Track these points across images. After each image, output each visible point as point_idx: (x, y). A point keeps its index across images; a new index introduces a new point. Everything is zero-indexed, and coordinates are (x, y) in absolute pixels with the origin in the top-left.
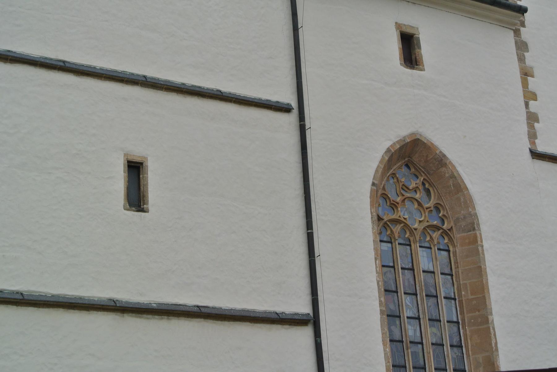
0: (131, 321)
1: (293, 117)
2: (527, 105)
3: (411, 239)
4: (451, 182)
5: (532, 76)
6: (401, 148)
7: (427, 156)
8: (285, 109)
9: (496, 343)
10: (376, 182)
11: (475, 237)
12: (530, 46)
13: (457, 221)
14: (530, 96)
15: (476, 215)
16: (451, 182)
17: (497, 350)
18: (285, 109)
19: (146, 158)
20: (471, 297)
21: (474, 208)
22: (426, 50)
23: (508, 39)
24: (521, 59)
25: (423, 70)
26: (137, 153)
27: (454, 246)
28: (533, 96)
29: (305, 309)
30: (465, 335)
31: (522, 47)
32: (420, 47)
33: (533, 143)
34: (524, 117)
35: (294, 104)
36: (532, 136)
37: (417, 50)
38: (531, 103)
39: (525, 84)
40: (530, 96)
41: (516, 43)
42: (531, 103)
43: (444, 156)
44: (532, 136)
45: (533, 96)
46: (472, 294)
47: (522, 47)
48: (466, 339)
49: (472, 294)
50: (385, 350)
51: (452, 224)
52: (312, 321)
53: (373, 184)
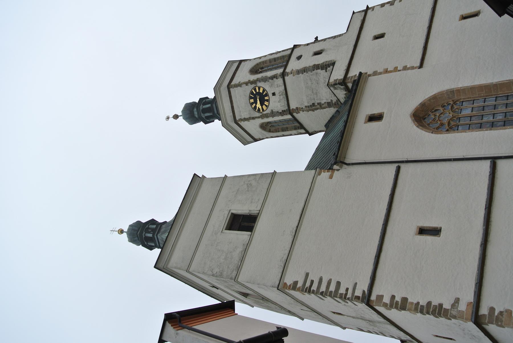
2: (399, 71)
6: (417, 121)
11: (457, 90)
13: (449, 98)
14: (396, 70)
17: (509, 80)
22: (376, 111)
24: (380, 73)
26: (414, 230)
27: (461, 99)
31: (375, 73)
33: (416, 68)
35: (397, 165)
36: (413, 68)
38: (399, 69)
39: (391, 72)
40: (396, 70)
41: (373, 76)
42: (399, 69)
44: (413, 68)
47: (375, 73)
52: (494, 160)
53: (432, 133)
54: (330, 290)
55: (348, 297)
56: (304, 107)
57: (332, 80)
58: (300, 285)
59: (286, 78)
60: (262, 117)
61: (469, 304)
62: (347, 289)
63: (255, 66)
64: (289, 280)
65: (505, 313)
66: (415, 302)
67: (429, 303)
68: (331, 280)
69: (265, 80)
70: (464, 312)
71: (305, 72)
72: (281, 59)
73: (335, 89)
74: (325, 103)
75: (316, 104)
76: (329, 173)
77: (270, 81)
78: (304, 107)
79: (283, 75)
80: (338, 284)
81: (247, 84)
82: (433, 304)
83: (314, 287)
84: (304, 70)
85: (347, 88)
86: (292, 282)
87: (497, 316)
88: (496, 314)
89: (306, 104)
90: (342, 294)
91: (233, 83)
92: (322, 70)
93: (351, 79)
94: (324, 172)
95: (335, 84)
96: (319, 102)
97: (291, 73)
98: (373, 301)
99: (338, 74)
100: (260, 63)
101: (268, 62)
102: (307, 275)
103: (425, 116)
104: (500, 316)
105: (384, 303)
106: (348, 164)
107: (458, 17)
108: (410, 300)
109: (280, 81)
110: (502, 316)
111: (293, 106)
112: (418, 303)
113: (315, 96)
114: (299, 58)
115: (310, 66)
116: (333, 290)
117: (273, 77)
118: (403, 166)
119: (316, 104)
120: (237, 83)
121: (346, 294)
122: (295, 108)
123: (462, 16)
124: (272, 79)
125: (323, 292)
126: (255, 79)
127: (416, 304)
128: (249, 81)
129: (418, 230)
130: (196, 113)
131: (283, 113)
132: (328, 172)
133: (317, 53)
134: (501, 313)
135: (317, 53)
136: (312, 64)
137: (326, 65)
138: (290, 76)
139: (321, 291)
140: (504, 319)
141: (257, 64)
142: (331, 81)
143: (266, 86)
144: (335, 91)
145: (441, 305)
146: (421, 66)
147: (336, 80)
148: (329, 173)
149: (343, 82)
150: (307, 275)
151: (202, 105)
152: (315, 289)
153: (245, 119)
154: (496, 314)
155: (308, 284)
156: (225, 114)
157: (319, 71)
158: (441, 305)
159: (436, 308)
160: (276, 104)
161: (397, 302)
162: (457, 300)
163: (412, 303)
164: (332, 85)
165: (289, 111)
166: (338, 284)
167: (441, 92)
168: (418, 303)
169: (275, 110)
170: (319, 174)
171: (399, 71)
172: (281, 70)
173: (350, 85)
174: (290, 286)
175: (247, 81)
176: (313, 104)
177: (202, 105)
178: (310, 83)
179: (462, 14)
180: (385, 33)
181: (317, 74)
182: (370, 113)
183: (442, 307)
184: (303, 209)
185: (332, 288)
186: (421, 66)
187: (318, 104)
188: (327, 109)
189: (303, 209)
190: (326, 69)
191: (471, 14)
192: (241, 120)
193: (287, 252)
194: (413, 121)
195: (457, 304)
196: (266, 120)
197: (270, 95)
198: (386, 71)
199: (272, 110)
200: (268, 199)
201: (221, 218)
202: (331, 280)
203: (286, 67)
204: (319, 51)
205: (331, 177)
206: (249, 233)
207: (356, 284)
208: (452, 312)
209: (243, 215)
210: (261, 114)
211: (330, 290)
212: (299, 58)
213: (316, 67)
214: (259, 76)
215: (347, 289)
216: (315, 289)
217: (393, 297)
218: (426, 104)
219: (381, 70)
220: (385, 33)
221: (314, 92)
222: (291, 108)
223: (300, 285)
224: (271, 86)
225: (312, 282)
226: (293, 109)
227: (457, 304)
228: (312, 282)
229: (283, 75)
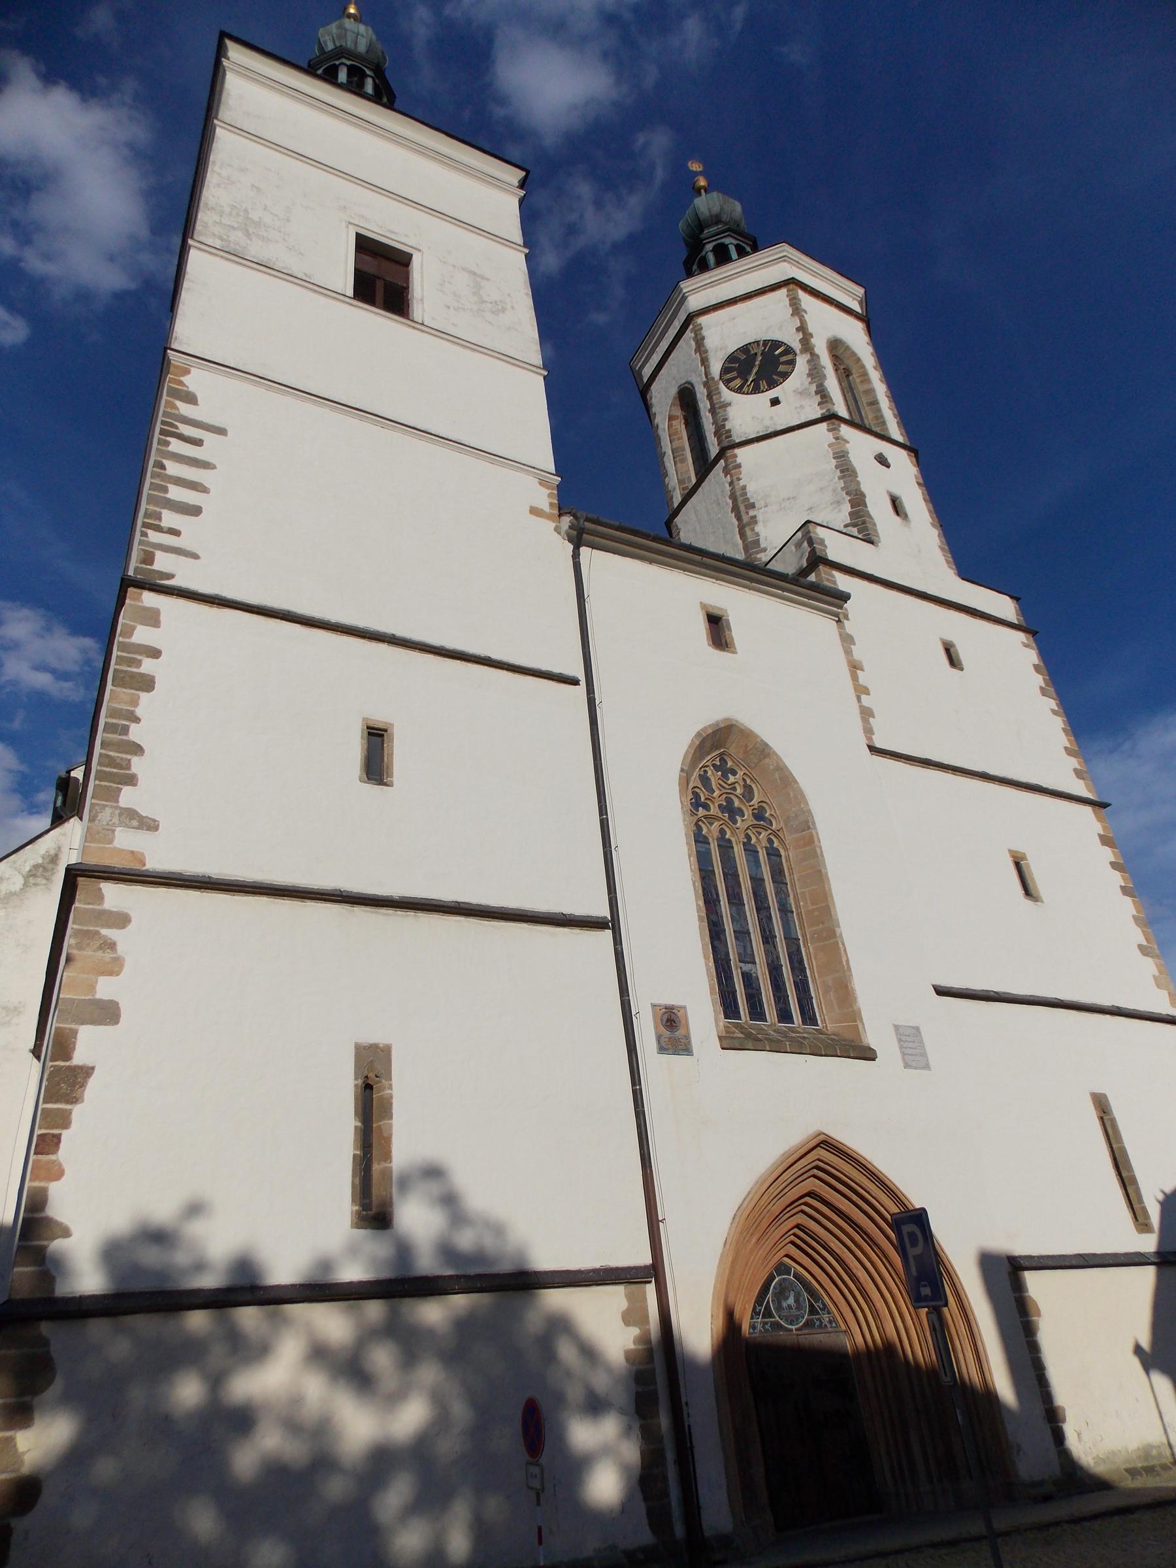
0: (360, 911)
1: (582, 688)
2: (859, 699)
3: (733, 839)
4: (777, 775)
5: (863, 670)
6: (714, 733)
7: (746, 746)
8: (574, 682)
9: (848, 961)
10: (686, 768)
11: (811, 836)
12: (856, 640)
13: (787, 821)
14: (861, 691)
15: (809, 811)
16: (777, 775)
17: (849, 968)
18: (574, 682)
19: (392, 725)
20: (811, 907)
21: (807, 804)
22: (737, 632)
23: (829, 624)
24: (848, 652)
25: (735, 652)
26: (379, 717)
27: (786, 849)
28: (798, 329)
29: (604, 912)
30: (808, 954)
31: (847, 640)
32: (730, 630)
33: (870, 739)
34: (856, 710)
35: (581, 676)
36: (868, 731)
37: (727, 632)
38: (863, 697)
39: (855, 678)
40: (861, 691)
41: (841, 635)
42: (863, 697)
43: (767, 745)
44: (868, 731)
45: (866, 691)
46: (813, 904)
47: (847, 640)
48: (809, 959)
49: (813, 904)
50: (707, 965)
51: (782, 824)
52: (611, 924)
53: (682, 770)
54: (171, 487)
55: (150, 532)
56: (742, 483)
57: (821, 532)
59: (823, 426)
60: (708, 383)
61: (139, 857)
63: (854, 354)
65: (108, 956)
66: (139, 712)
67: (137, 749)
68: (205, 490)
69: (815, 373)
70: (111, 841)
71: (842, 471)
72: (877, 418)
73: (798, 545)
74: (758, 534)
75: (752, 513)
76: (547, 508)
77: (814, 388)
78: (742, 483)
79: (830, 417)
81: (802, 328)
82: (135, 760)
84: (846, 470)
85: (804, 572)
86: (191, 389)
87: (97, 933)
88: (104, 932)
89: (749, 489)
90: (160, 519)
91: (801, 294)
92: (851, 514)
93: (828, 580)
94: (550, 495)
95: (811, 542)
96: (760, 518)
97: (837, 438)
98: (139, 598)
99: (838, 548)
100: (863, 367)
101: (866, 387)
102: (221, 431)
103: (730, 780)
104: (98, 943)
105: (133, 628)
106: (576, 556)
107: (1020, 847)
108: (144, 697)
109: (817, 413)
110: (100, 948)
111: (742, 454)
112: (137, 720)
114: (882, 460)
115: (858, 483)
116: (169, 496)
117: (823, 395)
119: (752, 513)
120: (804, 306)
121: (159, 529)
122: (739, 460)
123: (1024, 858)
125: (163, 467)
126: (817, 350)
127: (132, 713)
128: (811, 335)
129: (381, 726)
130: (713, 229)
131: (721, 431)
132: (551, 504)
134: (112, 946)
135: (896, 505)
136: (864, 488)
137: (864, 522)
138: (830, 438)
139: (166, 462)
140: (88, 952)
141: (859, 360)
142: (819, 530)
143: (799, 377)
144: (792, 547)
145: (131, 780)
146: (873, 749)
147: (822, 542)
148: (547, 508)
149: (817, 560)
150: (221, 431)
151: (736, 242)
152: (170, 448)
153: (700, 342)
154: (104, 932)
155: (185, 430)
156: (712, 284)
157: (847, 508)
158: (131, 780)
159: (122, 768)
160: (746, 412)
161: (139, 663)
162: (150, 825)
163: (135, 702)
164: (809, 532)
165: (728, 447)
166: (195, 511)
167: (803, 796)
168: (137, 720)
169: (732, 412)
170: (543, 483)
172: (843, 412)
173: (812, 578)
175: (810, 330)
176: (753, 506)
177: (736, 242)
179: (1028, 857)
180: (962, 669)
182: (731, 619)
183: (126, 784)
186: (873, 749)
187: (755, 517)
188: (740, 542)
190: (854, 525)
191: (1029, 882)
192: (698, 331)
194: (717, 723)
195: (135, 823)
196: (701, 393)
197: (772, 393)
198: (855, 667)
199: (730, 404)
200: (458, 348)
201: (393, 226)
202: (205, 490)
203: (850, 423)
204: (903, 507)
205: (535, 511)
206: (350, 292)
207: (196, 557)
208: (108, 811)
209: (407, 288)
210: (717, 377)
211: (171, 487)
212: (882, 460)
213: (858, 501)
214: (826, 360)
216: (170, 448)
217: (155, 653)
218: (767, 761)
219: (858, 652)
220: (962, 669)
222: (737, 451)
224: (802, 393)
225: (198, 443)
226: (736, 456)
227: (135, 823)
228: (198, 443)
229: (830, 417)
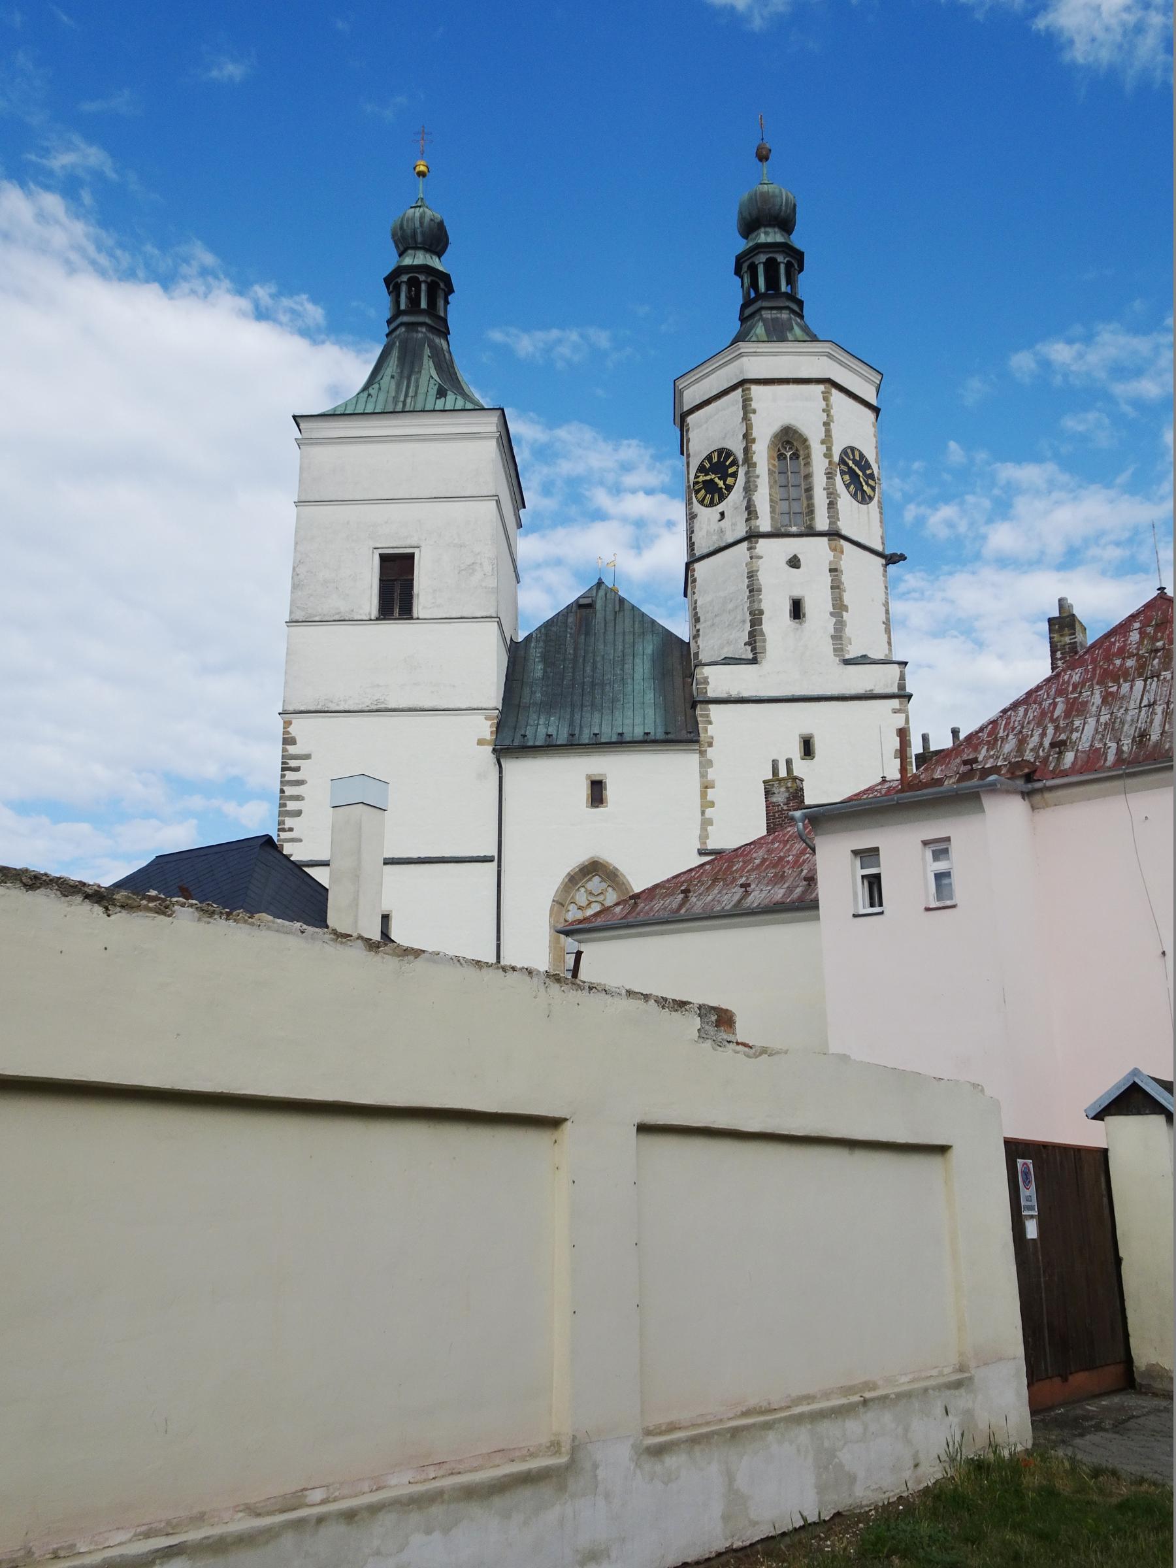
2: (703, 813)
58: (292, 750)
62: (291, 830)
63: (801, 435)
64: (299, 727)
77: (745, 504)
80: (298, 813)
83: (290, 776)
102: (307, 757)
113: (709, 623)
115: (760, 601)
118: (895, 690)
124: (747, 508)
133: (797, 610)
150: (307, 757)
157: (748, 627)
166: (298, 813)
171: (703, 813)
174: (288, 733)
178: (730, 606)
181: (744, 621)
184: (415, 710)
185: (292, 806)
189: (415, 710)
193: (341, 708)
198: (706, 786)
207: (300, 840)
215: (291, 830)
216: (287, 778)
221: (717, 620)
223: (292, 750)
225: (297, 769)
228: (297, 769)
